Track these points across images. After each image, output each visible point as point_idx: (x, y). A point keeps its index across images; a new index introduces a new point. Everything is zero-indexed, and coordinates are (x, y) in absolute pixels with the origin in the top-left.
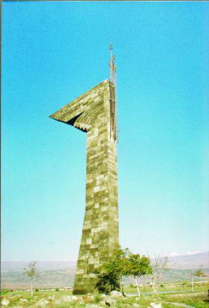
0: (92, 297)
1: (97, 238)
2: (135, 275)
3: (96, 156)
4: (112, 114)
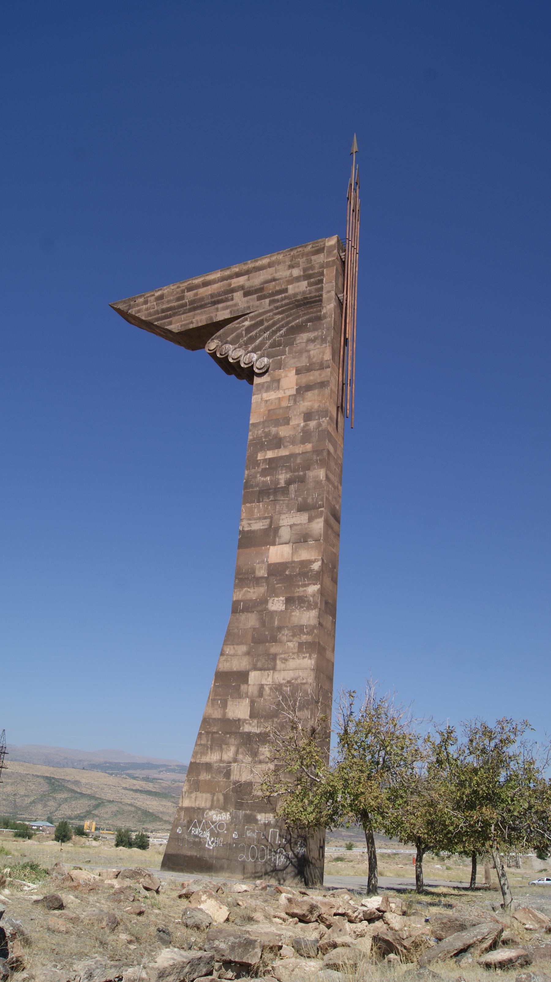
3: (283, 452)
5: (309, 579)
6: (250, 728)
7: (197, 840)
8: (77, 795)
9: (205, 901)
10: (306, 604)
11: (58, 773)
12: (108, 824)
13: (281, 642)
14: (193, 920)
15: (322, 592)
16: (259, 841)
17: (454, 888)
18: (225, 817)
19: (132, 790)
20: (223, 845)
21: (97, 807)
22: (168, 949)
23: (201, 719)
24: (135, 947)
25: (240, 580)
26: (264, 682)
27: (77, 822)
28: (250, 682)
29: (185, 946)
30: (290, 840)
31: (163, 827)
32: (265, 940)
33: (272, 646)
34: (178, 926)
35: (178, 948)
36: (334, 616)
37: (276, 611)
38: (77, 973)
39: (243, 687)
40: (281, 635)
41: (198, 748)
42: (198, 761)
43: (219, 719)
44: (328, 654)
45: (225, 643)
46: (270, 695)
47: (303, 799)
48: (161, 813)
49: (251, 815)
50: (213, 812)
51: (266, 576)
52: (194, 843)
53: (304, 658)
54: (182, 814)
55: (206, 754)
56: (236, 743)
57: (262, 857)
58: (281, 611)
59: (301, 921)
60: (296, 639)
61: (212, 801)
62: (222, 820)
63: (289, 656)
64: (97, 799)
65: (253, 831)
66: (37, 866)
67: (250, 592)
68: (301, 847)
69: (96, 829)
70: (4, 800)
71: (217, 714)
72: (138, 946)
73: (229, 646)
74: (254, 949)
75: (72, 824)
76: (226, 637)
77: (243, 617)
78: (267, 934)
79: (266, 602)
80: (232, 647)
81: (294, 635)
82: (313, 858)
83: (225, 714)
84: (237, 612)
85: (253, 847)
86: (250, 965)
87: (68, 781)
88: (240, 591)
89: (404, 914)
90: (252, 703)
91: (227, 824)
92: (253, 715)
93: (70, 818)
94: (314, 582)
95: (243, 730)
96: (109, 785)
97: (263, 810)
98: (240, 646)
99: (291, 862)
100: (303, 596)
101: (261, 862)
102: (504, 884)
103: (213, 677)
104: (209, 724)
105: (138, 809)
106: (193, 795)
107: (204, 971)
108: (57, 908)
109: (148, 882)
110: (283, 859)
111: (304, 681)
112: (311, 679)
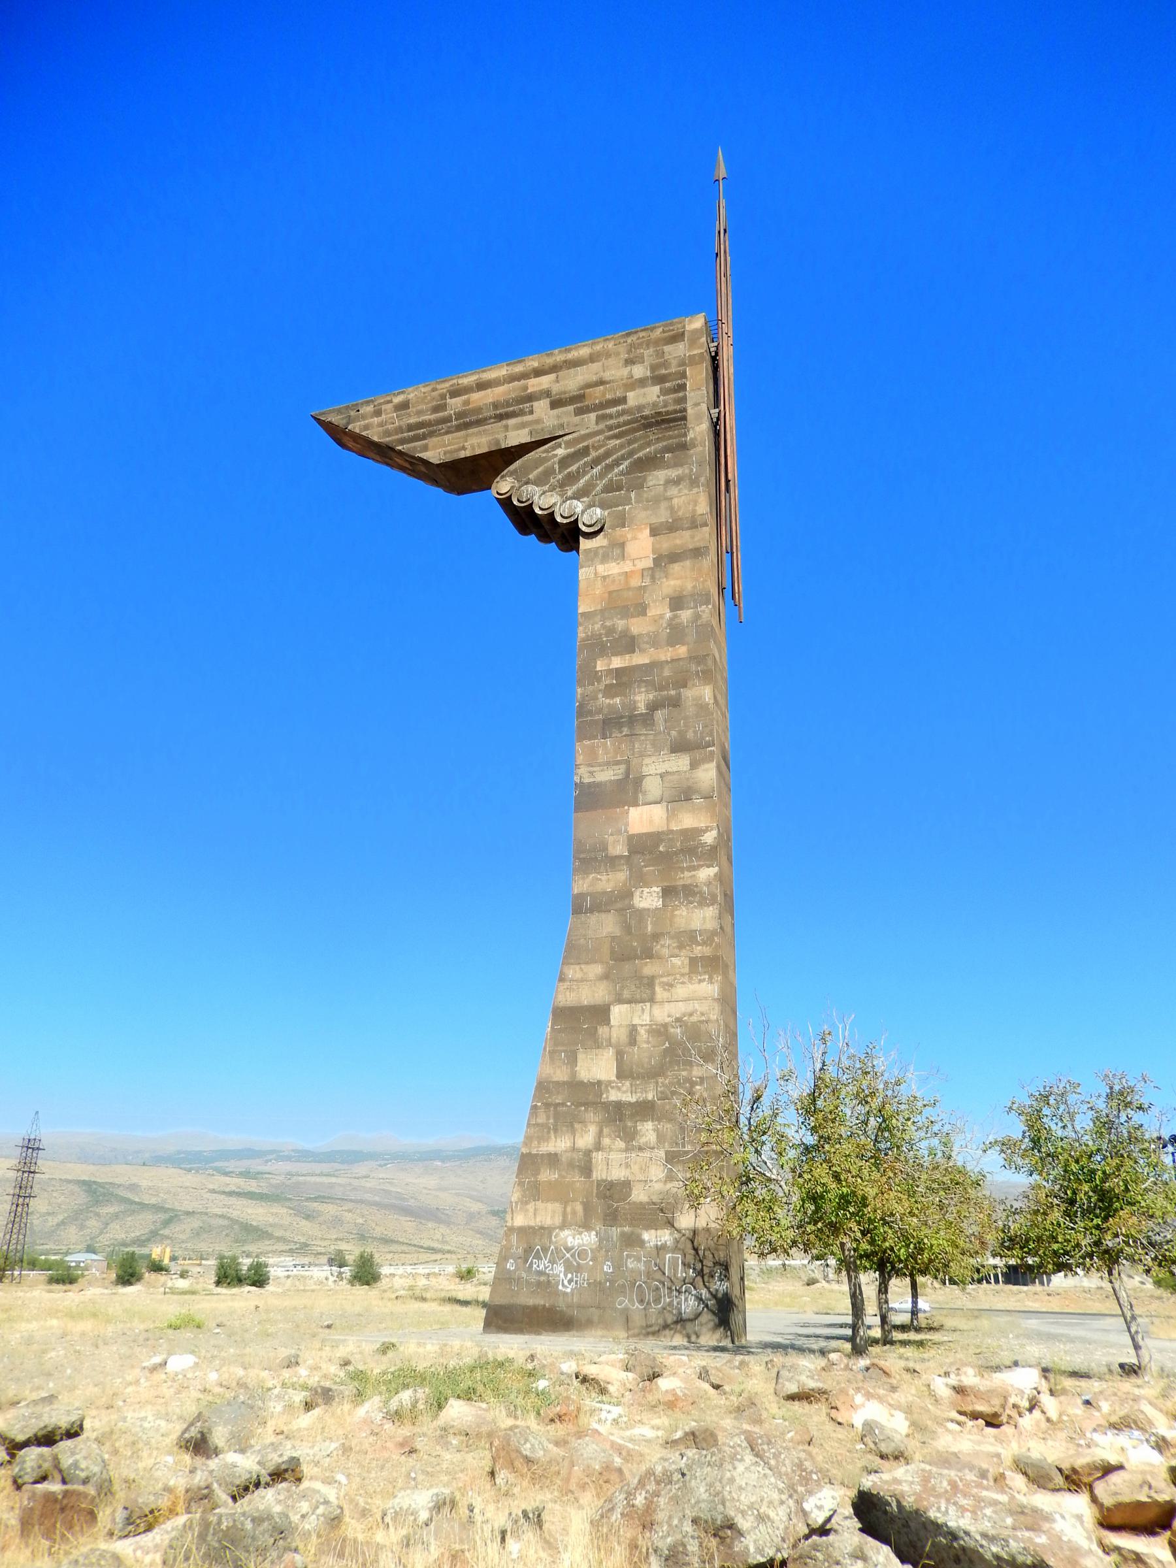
0: (781, 1485)
1: (646, 1050)
3: (639, 659)
5: (699, 858)
6: (619, 1094)
7: (542, 1278)
8: (133, 1207)
9: (863, 1405)
10: (697, 899)
11: (102, 1175)
12: (186, 1249)
13: (659, 957)
15: (719, 877)
16: (648, 1274)
18: (588, 1239)
19: (224, 1193)
20: (589, 1284)
21: (167, 1223)
25: (581, 860)
26: (636, 1021)
28: (613, 1022)
30: (702, 1270)
31: (275, 1248)
33: (646, 964)
37: (649, 909)
39: (602, 1031)
42: (534, 1152)
43: (564, 1083)
46: (648, 1042)
48: (271, 1225)
49: (632, 1233)
50: (566, 1232)
52: (539, 1284)
53: (700, 981)
54: (514, 1238)
55: (548, 1140)
57: (657, 1300)
58: (657, 909)
61: (564, 1214)
62: (583, 1245)
63: (675, 979)
64: (166, 1210)
65: (639, 1260)
67: (600, 880)
71: (561, 1074)
77: (593, 919)
79: (630, 895)
80: (577, 967)
81: (681, 947)
83: (574, 1074)
84: (581, 912)
85: (641, 1285)
87: (119, 1186)
88: (583, 879)
90: (620, 1055)
92: (620, 1075)
95: (607, 1097)
97: (652, 1225)
98: (593, 966)
100: (691, 885)
101: (654, 1309)
102: (1137, 1332)
104: (548, 1090)
106: (531, 1207)
110: (692, 1302)
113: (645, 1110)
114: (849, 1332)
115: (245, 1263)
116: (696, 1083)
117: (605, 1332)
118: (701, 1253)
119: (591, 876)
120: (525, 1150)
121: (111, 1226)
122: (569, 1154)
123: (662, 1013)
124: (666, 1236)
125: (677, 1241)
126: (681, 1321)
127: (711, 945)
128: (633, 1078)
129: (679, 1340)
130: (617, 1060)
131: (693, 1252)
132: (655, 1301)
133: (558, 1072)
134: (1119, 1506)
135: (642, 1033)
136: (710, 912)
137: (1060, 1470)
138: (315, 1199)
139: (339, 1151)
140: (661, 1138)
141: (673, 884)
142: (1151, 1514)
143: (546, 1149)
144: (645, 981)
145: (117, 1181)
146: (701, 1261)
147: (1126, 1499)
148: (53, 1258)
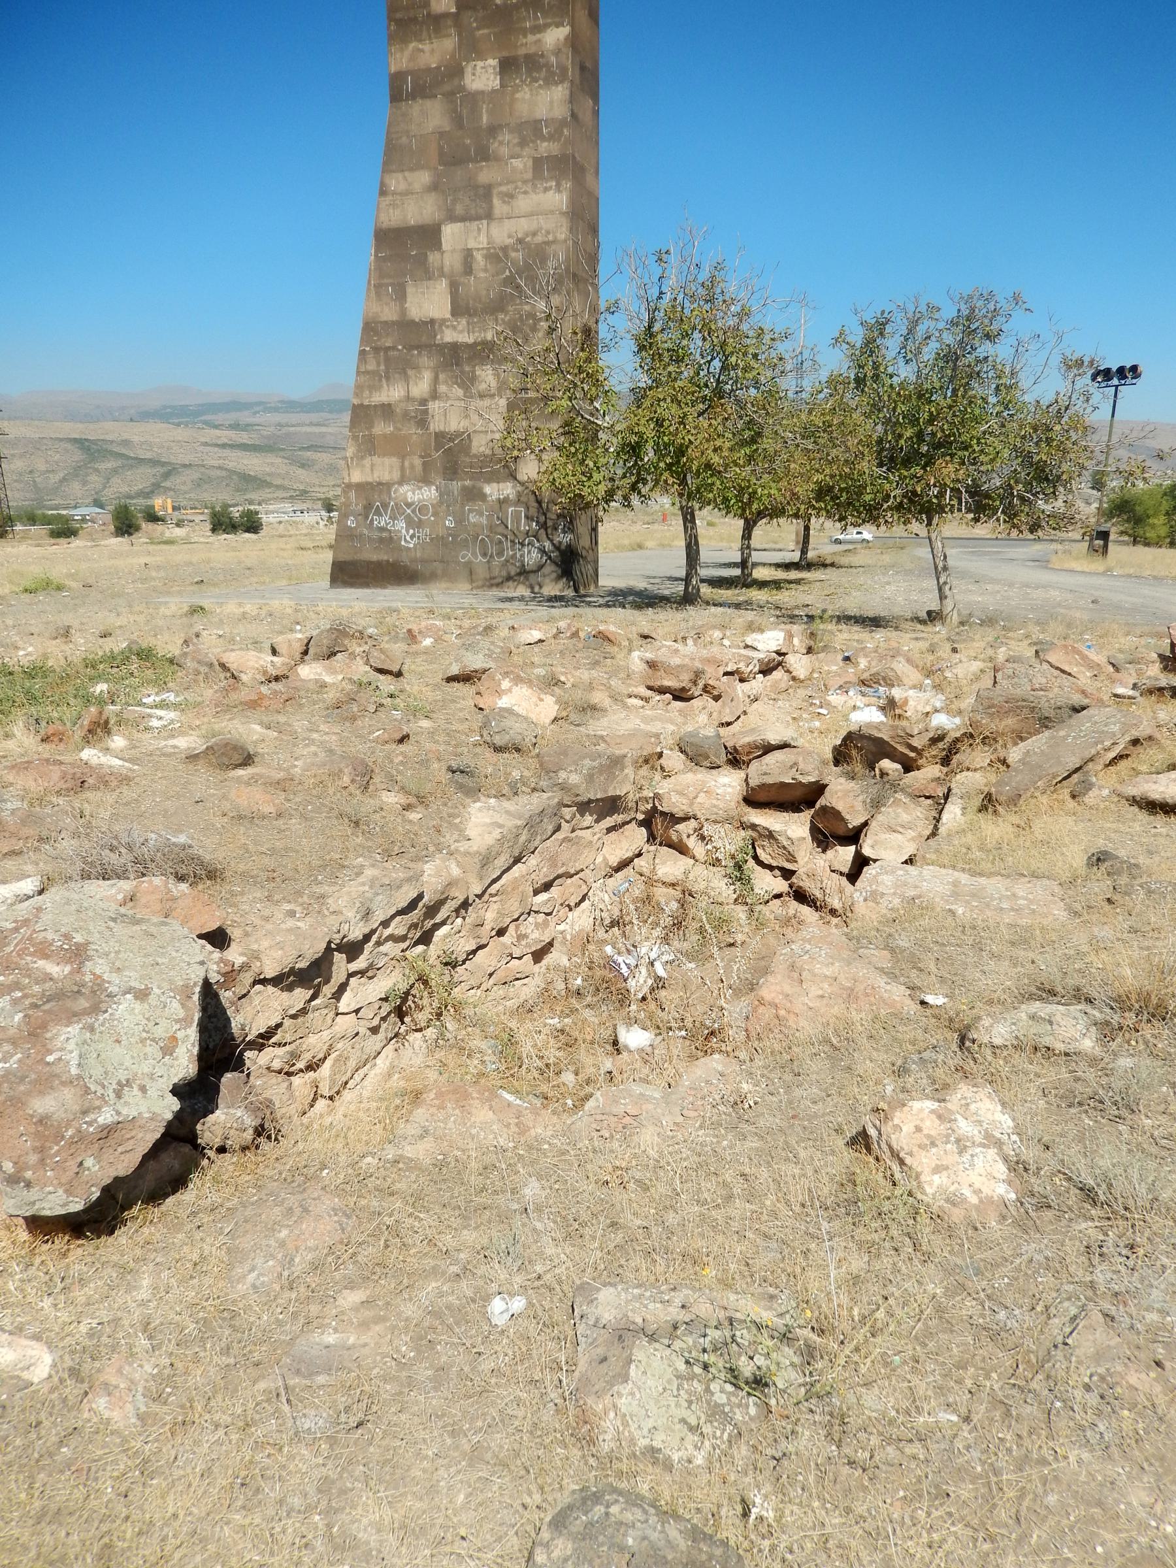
1: (483, 274)
2: (235, 1315)
4: (875, 622)
5: (545, 14)
6: (455, 334)
7: (384, 535)
8: (130, 462)
9: (510, 690)
10: (543, 74)
11: (92, 432)
12: (190, 499)
13: (498, 159)
14: (507, 737)
15: (573, 41)
16: (491, 528)
17: (778, 566)
18: (428, 494)
19: (217, 445)
20: (431, 539)
21: (166, 475)
22: (478, 805)
23: (360, 325)
24: (420, 816)
25: (399, 23)
26: (471, 244)
27: (142, 502)
28: (445, 246)
29: (506, 790)
30: (545, 523)
31: (275, 495)
32: (630, 750)
33: (481, 168)
34: (478, 750)
35: (495, 797)
36: (595, 97)
37: (482, 92)
38: (341, 918)
39: (433, 258)
40: (496, 145)
41: (362, 379)
42: (366, 403)
43: (393, 323)
44: (589, 178)
45: (387, 168)
46: (486, 270)
47: (584, 460)
48: (269, 475)
49: (474, 487)
50: (406, 488)
51: (454, 10)
52: (381, 540)
53: (546, 190)
54: (352, 494)
55: (379, 388)
56: (432, 364)
57: (500, 553)
58: (494, 91)
59: (676, 698)
60: (527, 151)
61: (402, 468)
62: (424, 500)
63: (516, 188)
64: (163, 464)
65: (481, 514)
66: (150, 650)
67: (422, 51)
68: (564, 532)
69: (174, 508)
70: (16, 481)
71: (389, 313)
72: (426, 812)
73: (394, 175)
74: (622, 770)
75: (135, 504)
76: (385, 154)
77: (416, 108)
78: (633, 734)
79: (458, 72)
80: (400, 176)
81: (523, 143)
82: (584, 548)
83: (403, 311)
84: (402, 100)
85: (483, 540)
86: (619, 797)
87: (112, 442)
88: (402, 50)
89: (810, 650)
90: (454, 287)
91: (433, 506)
92: (456, 312)
93: (130, 497)
94: (557, 20)
95: (442, 339)
96: (179, 441)
97: (493, 478)
98: (417, 174)
99: (550, 558)
100: (536, 54)
101: (497, 561)
102: (945, 583)
103: (371, 241)
104: (377, 333)
105: (232, 472)
106: (367, 462)
107: (550, 828)
108: (240, 765)
109: (379, 658)
110: (535, 554)
111: (551, 238)
112: (562, 234)
113: (483, 352)
114: (737, 572)
115: (235, 512)
116: (540, 319)
117: (448, 585)
118: (544, 505)
119: (412, 45)
120: (356, 401)
121: (113, 480)
122: (403, 405)
123: (501, 233)
124: (508, 489)
125: (519, 495)
126: (524, 573)
127: (559, 140)
128: (470, 315)
129: (522, 591)
130: (451, 293)
131: (536, 505)
132: (498, 554)
133: (386, 310)
134: (763, 786)
135: (479, 258)
136: (559, 92)
137: (726, 748)
138: (308, 448)
139: (327, 401)
140: (502, 386)
141: (513, 54)
142: (798, 793)
143: (378, 399)
144: (481, 191)
145: (108, 437)
146: (545, 514)
147: (770, 780)
148: (50, 512)
